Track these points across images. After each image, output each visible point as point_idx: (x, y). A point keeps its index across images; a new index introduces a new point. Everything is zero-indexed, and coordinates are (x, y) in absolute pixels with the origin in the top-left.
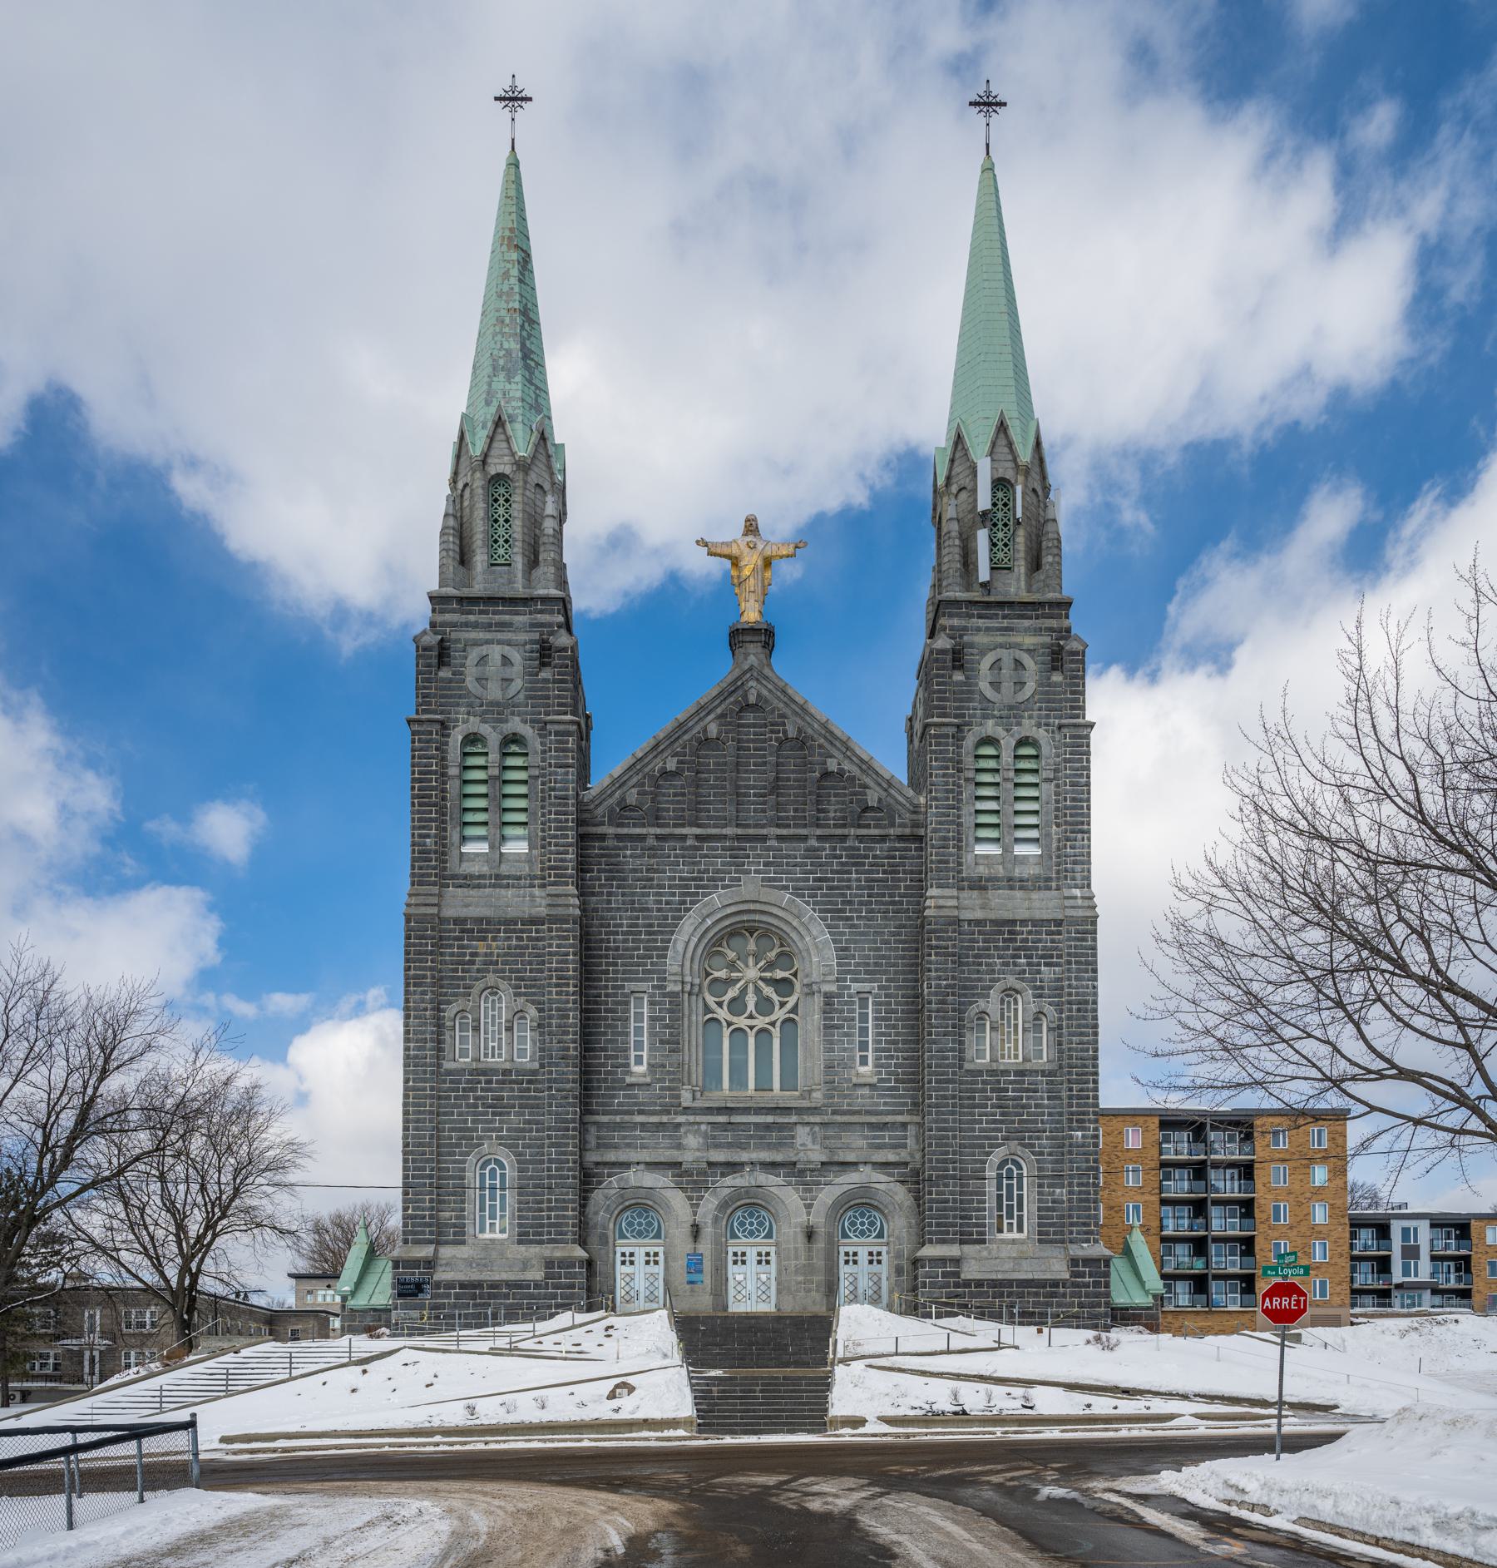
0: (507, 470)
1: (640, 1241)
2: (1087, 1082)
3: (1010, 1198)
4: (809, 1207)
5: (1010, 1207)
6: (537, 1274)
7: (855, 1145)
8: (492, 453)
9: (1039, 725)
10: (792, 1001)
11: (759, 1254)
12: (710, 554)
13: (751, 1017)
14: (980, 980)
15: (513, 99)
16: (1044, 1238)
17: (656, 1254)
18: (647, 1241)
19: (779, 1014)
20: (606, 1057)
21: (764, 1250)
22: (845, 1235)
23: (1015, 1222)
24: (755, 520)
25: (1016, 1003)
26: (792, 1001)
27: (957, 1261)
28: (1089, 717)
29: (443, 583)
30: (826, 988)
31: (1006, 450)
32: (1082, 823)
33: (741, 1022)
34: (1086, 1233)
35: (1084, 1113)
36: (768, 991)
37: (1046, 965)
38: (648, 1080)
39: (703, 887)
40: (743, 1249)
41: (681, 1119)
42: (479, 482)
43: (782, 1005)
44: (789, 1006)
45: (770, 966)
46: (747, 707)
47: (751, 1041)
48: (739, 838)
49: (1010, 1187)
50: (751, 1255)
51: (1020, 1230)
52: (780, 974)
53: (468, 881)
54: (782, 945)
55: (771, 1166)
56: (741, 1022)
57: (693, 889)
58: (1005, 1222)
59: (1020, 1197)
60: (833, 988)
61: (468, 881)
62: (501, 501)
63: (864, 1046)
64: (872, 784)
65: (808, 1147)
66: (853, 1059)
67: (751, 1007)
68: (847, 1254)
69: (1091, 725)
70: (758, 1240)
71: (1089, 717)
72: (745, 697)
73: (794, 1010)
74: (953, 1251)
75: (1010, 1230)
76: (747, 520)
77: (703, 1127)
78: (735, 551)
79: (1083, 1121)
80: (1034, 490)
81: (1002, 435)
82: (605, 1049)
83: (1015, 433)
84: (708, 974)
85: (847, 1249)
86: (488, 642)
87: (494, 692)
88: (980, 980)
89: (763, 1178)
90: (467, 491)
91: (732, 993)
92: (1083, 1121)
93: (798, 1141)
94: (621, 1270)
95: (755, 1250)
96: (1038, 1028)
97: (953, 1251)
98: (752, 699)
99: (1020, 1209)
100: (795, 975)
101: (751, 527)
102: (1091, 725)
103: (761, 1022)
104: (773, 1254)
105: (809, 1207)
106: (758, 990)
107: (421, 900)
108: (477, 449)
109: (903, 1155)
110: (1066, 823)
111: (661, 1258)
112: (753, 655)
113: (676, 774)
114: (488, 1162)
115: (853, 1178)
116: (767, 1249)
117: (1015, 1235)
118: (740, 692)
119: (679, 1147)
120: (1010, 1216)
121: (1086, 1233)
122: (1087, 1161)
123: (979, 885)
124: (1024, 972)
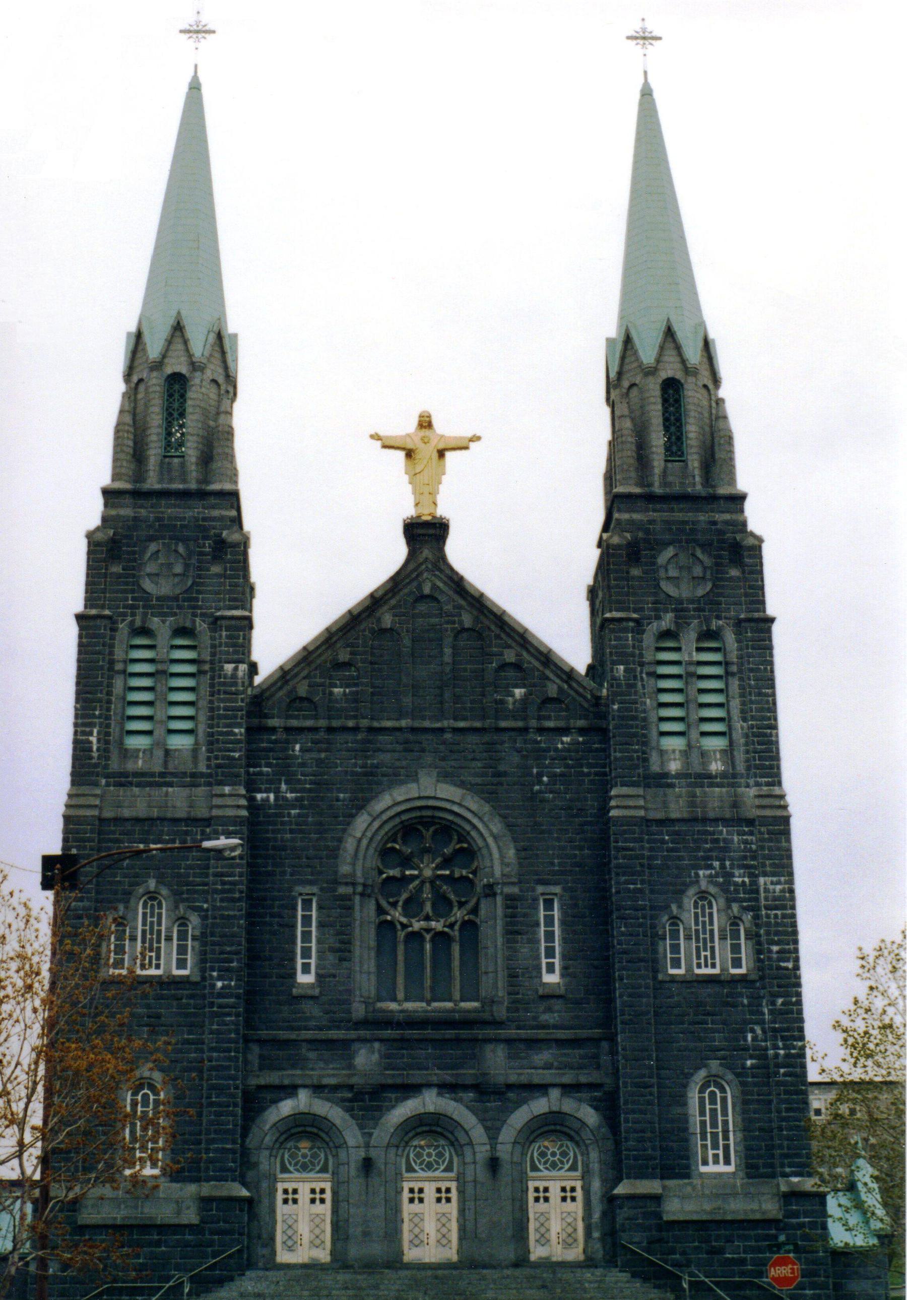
0: (184, 370)
1: (305, 1175)
3: (714, 1125)
5: (715, 1136)
6: (191, 1216)
7: (541, 1064)
8: (170, 353)
11: (439, 1190)
12: (385, 447)
13: (427, 918)
15: (198, 31)
17: (322, 1191)
18: (312, 1175)
19: (459, 914)
21: (443, 1186)
22: (535, 1168)
23: (721, 1152)
24: (429, 416)
25: (711, 907)
27: (657, 1199)
29: (115, 476)
30: (508, 890)
31: (674, 353)
32: (769, 719)
35: (788, 1030)
38: (317, 992)
40: (546, 1184)
42: (156, 382)
46: (422, 598)
48: (413, 730)
50: (430, 1191)
58: (711, 1152)
60: (515, 890)
62: (176, 396)
63: (550, 953)
64: (551, 676)
65: (497, 1063)
66: (538, 968)
68: (412, 1191)
70: (437, 1174)
72: (419, 588)
74: (652, 1186)
75: (716, 1161)
76: (421, 416)
77: (448, 736)
78: (410, 446)
80: (705, 386)
81: (670, 339)
82: (270, 959)
83: (682, 335)
85: (537, 1184)
90: (142, 388)
94: (281, 1210)
95: (434, 1185)
96: (736, 935)
97: (652, 1186)
98: (427, 590)
99: (726, 1138)
101: (425, 423)
102: (772, 620)
104: (579, 1189)
106: (435, 889)
107: (81, 801)
108: (154, 349)
109: (594, 1077)
110: (753, 718)
111: (328, 1196)
113: (347, 665)
114: (141, 1087)
115: (540, 1106)
116: (573, 1183)
118: (415, 584)
120: (715, 1146)
123: (144, 779)
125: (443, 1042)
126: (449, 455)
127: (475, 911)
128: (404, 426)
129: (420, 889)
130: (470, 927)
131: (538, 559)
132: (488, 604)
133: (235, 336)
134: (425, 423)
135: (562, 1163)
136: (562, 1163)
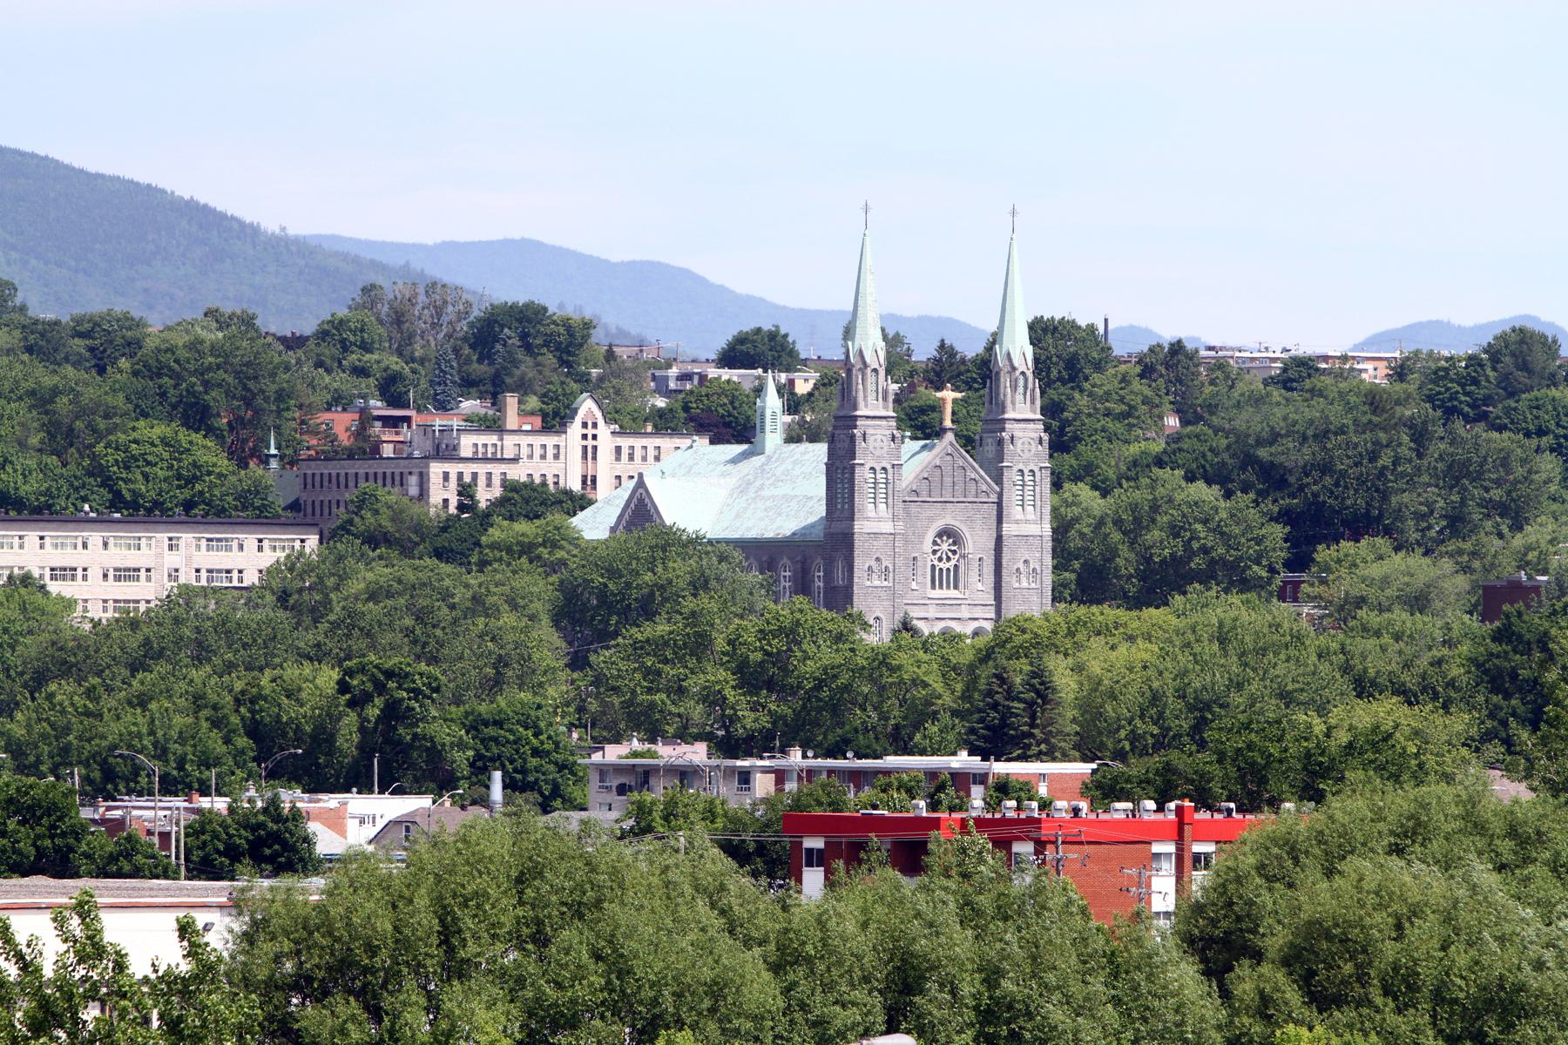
19: (953, 562)
33: (941, 565)
53: (868, 519)
56: (941, 565)
57: (931, 519)
61: (868, 519)
87: (877, 453)
89: (953, 624)
123: (1017, 522)
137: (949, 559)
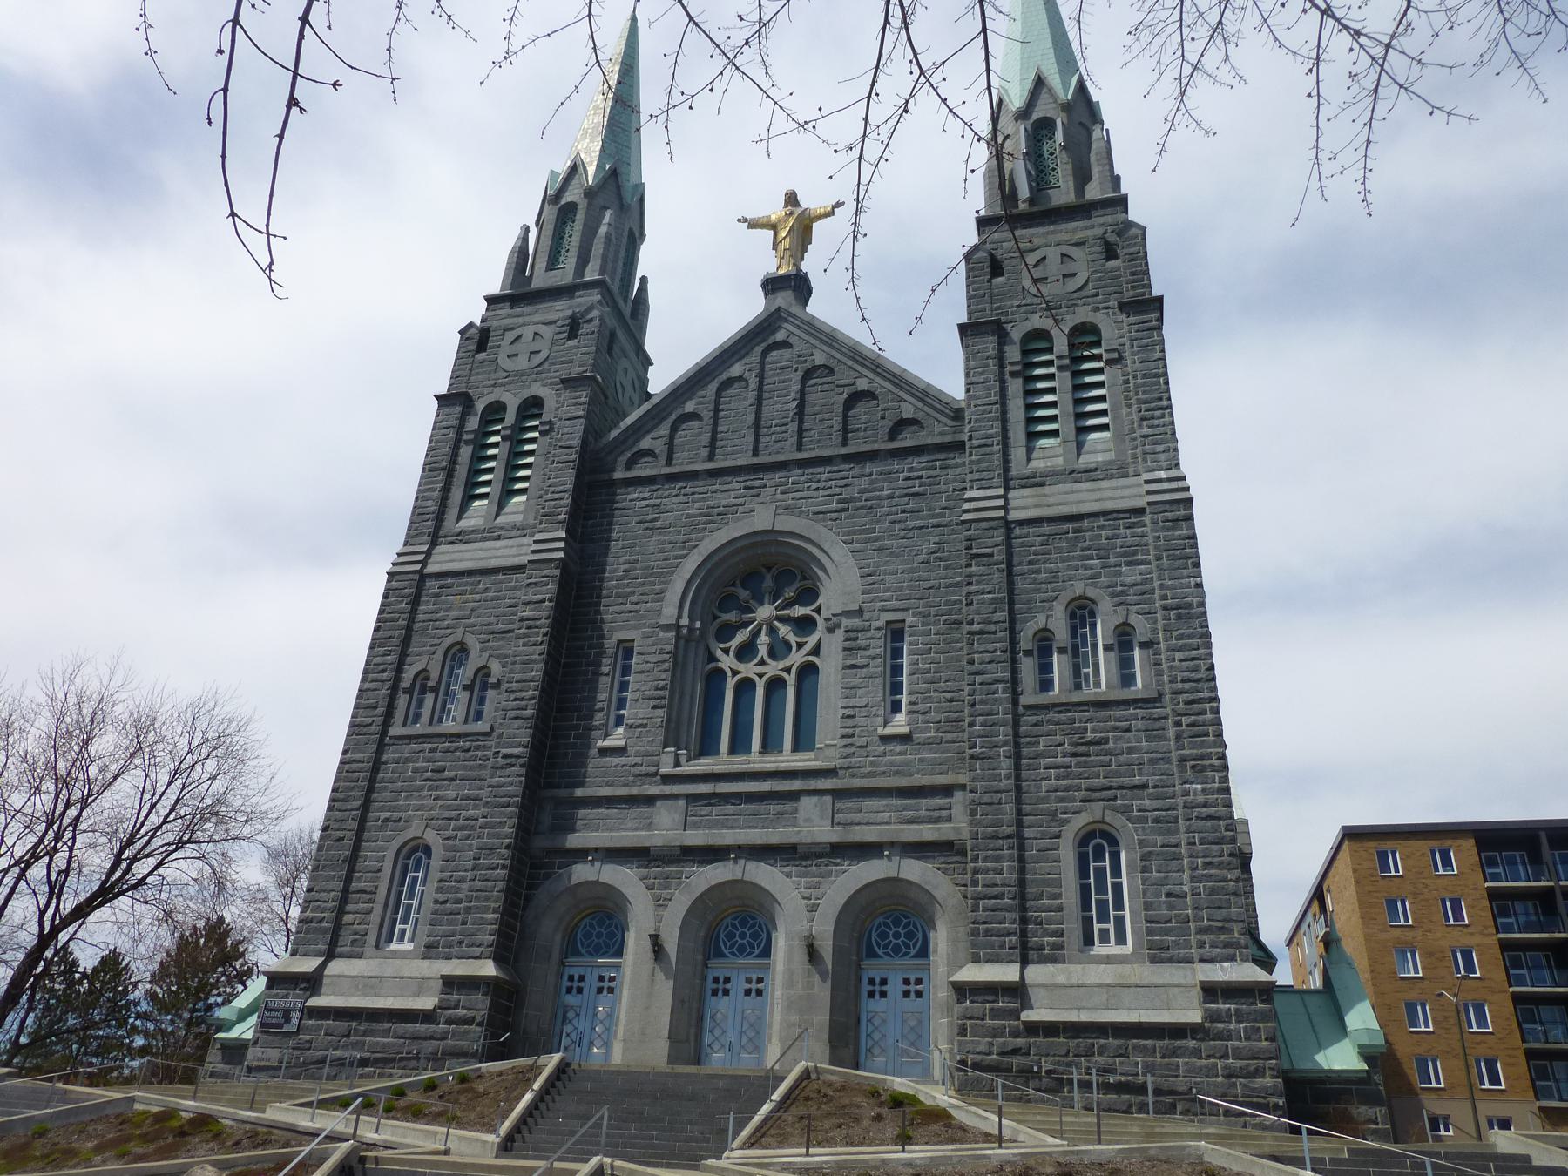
2: (1203, 712)
4: (813, 909)
5: (1102, 905)
9: (1097, 309)
10: (811, 641)
12: (750, 227)
14: (1038, 590)
16: (1159, 954)
19: (797, 658)
20: (579, 718)
23: (1111, 926)
26: (811, 641)
28: (1123, 191)
33: (749, 669)
34: (1227, 945)
35: (1202, 758)
36: (783, 630)
37: (1129, 564)
39: (712, 522)
41: (654, 790)
43: (800, 646)
44: (808, 647)
45: (789, 604)
47: (760, 693)
49: (1100, 873)
51: (1121, 940)
52: (799, 611)
54: (804, 578)
55: (919, 849)
56: (749, 669)
59: (1118, 888)
67: (763, 651)
69: (1160, 299)
71: (1156, 292)
73: (816, 651)
75: (1105, 939)
79: (1204, 768)
82: (578, 709)
84: (716, 618)
86: (524, 325)
88: (1038, 590)
91: (741, 637)
92: (1204, 768)
93: (801, 815)
99: (1119, 905)
100: (818, 610)
101: (791, 199)
103: (773, 668)
105: (813, 909)
106: (772, 631)
112: (784, 299)
117: (1112, 949)
119: (650, 826)
120: (1103, 918)
121: (1227, 945)
122: (1215, 829)
124: (1098, 576)
125: (693, 798)
126: (816, 226)
127: (816, 651)
128: (775, 209)
129: (772, 631)
130: (808, 671)
131: (906, 313)
132: (839, 337)
133: (1246, 823)
134: (791, 199)
135: (908, 946)
136: (908, 946)
137: (779, 649)
